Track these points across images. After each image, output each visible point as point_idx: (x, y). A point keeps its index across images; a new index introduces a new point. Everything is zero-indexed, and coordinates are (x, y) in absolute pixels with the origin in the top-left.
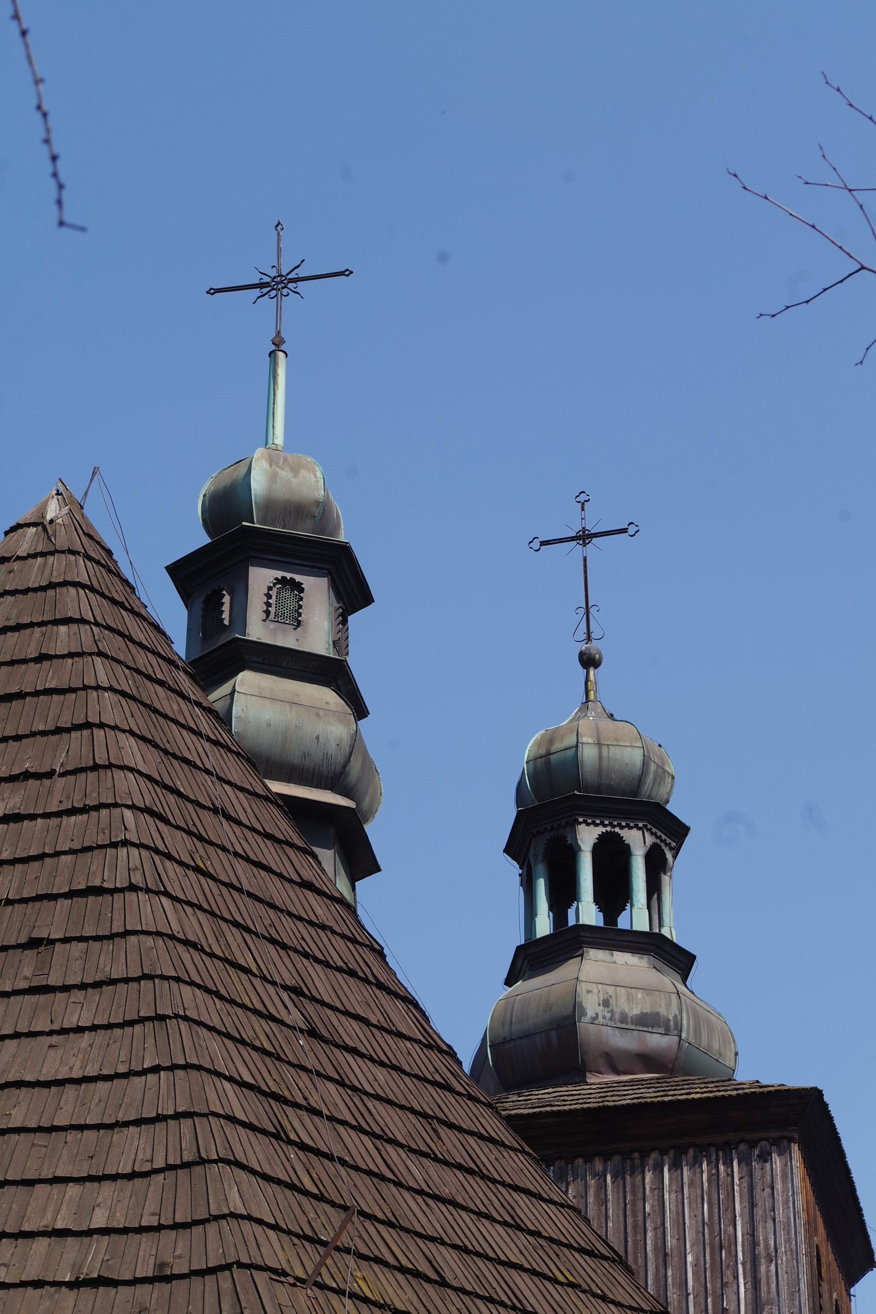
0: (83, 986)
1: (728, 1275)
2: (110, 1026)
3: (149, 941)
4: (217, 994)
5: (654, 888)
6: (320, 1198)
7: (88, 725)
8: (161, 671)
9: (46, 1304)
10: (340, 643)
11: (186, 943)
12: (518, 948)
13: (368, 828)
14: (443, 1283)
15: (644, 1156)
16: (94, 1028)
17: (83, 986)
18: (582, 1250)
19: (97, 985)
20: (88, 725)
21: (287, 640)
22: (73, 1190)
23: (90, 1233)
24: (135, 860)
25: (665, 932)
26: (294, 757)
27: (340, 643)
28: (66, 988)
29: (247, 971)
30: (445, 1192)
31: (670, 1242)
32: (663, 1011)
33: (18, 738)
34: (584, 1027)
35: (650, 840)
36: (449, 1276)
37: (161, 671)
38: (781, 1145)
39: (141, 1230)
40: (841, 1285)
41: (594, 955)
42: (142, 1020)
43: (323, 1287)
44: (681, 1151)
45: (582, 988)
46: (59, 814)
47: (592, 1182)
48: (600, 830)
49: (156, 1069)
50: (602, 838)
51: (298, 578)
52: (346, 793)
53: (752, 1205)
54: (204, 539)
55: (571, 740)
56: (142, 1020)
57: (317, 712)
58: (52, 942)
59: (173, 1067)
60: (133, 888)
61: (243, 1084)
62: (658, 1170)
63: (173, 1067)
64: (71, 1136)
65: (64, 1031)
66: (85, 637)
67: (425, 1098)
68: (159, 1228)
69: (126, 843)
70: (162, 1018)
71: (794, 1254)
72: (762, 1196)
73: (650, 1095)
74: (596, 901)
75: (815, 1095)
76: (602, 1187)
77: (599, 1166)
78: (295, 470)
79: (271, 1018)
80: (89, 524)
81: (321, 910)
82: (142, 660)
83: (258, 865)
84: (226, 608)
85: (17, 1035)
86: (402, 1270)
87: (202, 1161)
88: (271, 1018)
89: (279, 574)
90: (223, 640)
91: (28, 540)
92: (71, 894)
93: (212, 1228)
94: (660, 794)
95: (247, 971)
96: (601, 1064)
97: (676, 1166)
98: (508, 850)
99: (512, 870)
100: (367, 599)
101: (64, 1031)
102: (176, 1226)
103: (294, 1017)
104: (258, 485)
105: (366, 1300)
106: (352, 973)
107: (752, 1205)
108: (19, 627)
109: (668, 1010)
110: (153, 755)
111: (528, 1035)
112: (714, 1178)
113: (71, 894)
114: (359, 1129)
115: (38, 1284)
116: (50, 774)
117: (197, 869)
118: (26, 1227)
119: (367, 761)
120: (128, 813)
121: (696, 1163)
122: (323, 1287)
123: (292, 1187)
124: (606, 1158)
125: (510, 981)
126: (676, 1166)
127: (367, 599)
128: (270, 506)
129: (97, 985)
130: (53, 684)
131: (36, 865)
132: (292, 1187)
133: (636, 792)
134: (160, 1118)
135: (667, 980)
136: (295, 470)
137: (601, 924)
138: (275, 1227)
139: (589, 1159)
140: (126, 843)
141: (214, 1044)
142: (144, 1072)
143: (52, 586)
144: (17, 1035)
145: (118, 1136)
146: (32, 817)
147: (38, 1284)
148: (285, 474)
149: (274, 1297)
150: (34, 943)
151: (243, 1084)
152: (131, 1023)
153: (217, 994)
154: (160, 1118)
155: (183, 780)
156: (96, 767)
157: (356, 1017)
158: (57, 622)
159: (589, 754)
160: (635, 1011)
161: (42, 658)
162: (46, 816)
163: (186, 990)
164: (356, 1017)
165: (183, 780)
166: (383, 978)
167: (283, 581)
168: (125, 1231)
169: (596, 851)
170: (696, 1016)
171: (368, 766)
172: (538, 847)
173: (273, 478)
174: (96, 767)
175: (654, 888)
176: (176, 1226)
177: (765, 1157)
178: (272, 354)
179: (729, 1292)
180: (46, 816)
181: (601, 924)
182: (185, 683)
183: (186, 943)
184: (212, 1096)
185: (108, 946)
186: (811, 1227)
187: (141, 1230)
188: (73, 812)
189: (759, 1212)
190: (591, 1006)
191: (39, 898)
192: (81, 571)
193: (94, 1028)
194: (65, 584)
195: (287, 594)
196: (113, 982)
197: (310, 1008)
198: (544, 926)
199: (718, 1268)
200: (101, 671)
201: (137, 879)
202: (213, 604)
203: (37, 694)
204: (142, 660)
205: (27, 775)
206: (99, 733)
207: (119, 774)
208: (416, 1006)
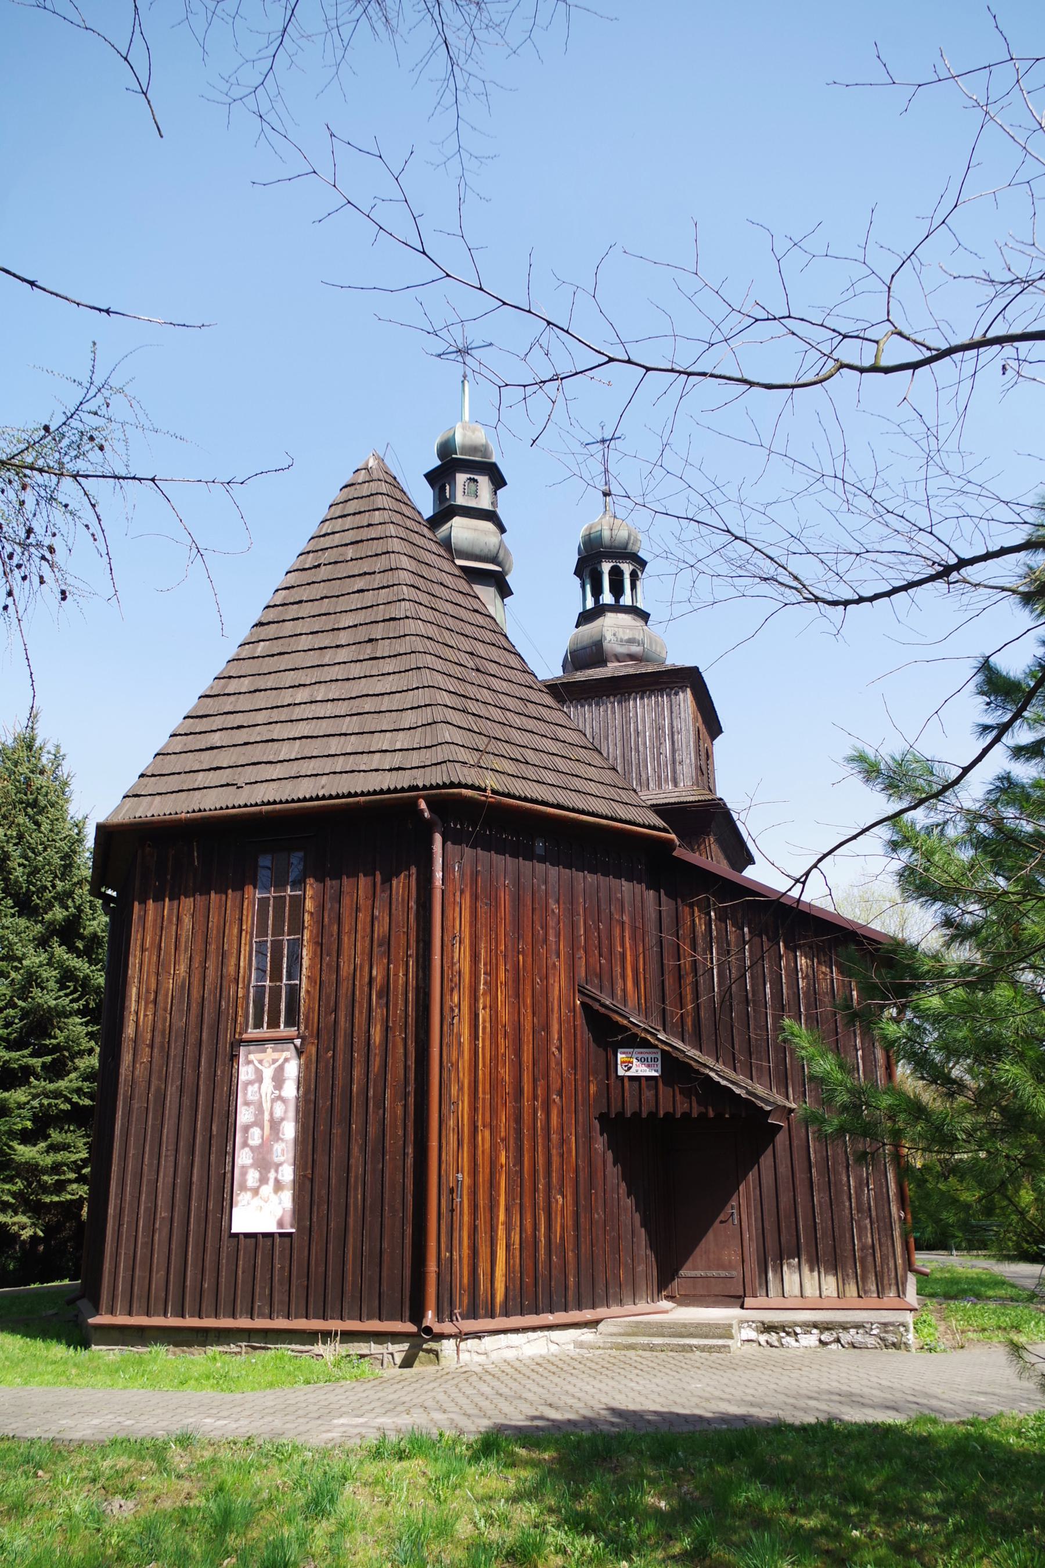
0: (390, 657)
1: (662, 740)
2: (400, 672)
3: (414, 638)
4: (440, 657)
5: (633, 587)
6: (480, 734)
7: (388, 552)
8: (416, 527)
9: (380, 777)
10: (494, 504)
11: (428, 638)
12: (580, 614)
13: (507, 578)
14: (527, 763)
15: (630, 695)
16: (394, 673)
17: (390, 657)
18: (582, 747)
19: (395, 656)
20: (388, 552)
21: (472, 503)
22: (388, 734)
23: (395, 751)
24: (408, 607)
25: (638, 605)
26: (477, 551)
27: (494, 504)
28: (383, 658)
29: (452, 647)
30: (529, 728)
31: (640, 728)
32: (637, 637)
33: (361, 558)
34: (606, 644)
35: (632, 567)
36: (529, 760)
37: (416, 527)
38: (683, 688)
39: (413, 749)
40: (708, 740)
41: (609, 615)
42: (412, 669)
43: (481, 767)
44: (644, 692)
45: (605, 629)
46: (378, 589)
47: (609, 706)
48: (612, 564)
49: (417, 688)
50: (613, 568)
51: (476, 477)
52: (499, 564)
53: (672, 712)
54: (439, 463)
55: (599, 528)
56: (412, 669)
57: (486, 532)
58: (377, 640)
59: (424, 687)
60: (407, 617)
61: (450, 692)
62: (635, 699)
63: (424, 687)
64: (387, 714)
65: (383, 675)
66: (385, 516)
67: (153, 986)
68: (420, 748)
69: (404, 600)
70: (419, 668)
71: (688, 730)
72: (675, 709)
73: (631, 671)
74: (611, 591)
75: (695, 670)
76: (613, 707)
77: (612, 699)
78: (473, 432)
79: (462, 665)
80: (386, 467)
81: (480, 620)
82: (409, 523)
83: (456, 604)
84: (448, 491)
85: (365, 677)
86: (511, 759)
87: (435, 723)
88: (462, 665)
89: (469, 476)
90: (447, 504)
91: (362, 476)
92: (384, 621)
93: (439, 747)
94: (635, 549)
95: (452, 647)
96: (613, 659)
97: (642, 698)
98: (575, 573)
99: (577, 581)
100: (505, 484)
101: (383, 675)
102: (426, 747)
103: (471, 664)
104: (459, 440)
105: (497, 771)
106: (494, 645)
107: (672, 712)
108: (360, 513)
109: (639, 636)
110: (414, 563)
111: (584, 648)
112: (657, 702)
113: (384, 621)
114: (496, 706)
115: (377, 770)
116: (374, 573)
117: (432, 608)
118: (372, 750)
119: (506, 550)
120: (404, 587)
121: (650, 697)
122: (481, 767)
123: (469, 730)
124: (615, 696)
125: (577, 627)
126: (642, 698)
127: (505, 484)
128: (465, 449)
129: (395, 656)
130: (373, 536)
131: (370, 609)
132: (469, 730)
133: (626, 548)
134: (419, 707)
135: (640, 623)
136: (473, 432)
137: (613, 602)
138: (463, 746)
139: (608, 697)
140: (404, 600)
141: (439, 677)
142: (413, 689)
143: (372, 495)
144: (365, 677)
145: (404, 714)
146: (368, 590)
147: (377, 770)
148: (469, 433)
149: (462, 772)
150: (370, 640)
151: (450, 692)
152: (408, 671)
153: (440, 657)
154: (419, 707)
155: (425, 571)
156: (391, 569)
157: (495, 662)
158: (374, 510)
159: (606, 534)
160: (626, 637)
161: (369, 525)
162: (373, 589)
163: (428, 656)
164: (495, 662)
165: (425, 571)
166: (506, 645)
167: (470, 479)
168: (408, 750)
169: (611, 573)
170: (650, 638)
171: (507, 553)
172: (587, 572)
173: (464, 435)
174: (391, 569)
175: (633, 587)
176: (426, 747)
177: (676, 694)
178: (463, 382)
179: (663, 746)
180: (373, 589)
181: (613, 602)
182: (426, 531)
183: (428, 638)
184: (438, 697)
185: (399, 640)
186: (695, 719)
187: (413, 749)
188: (383, 587)
189: (674, 715)
190: (609, 636)
191: (372, 623)
192: (384, 488)
193: (394, 673)
194: (377, 494)
195: (472, 484)
196: (401, 655)
197: (477, 660)
198: (590, 604)
199: (658, 737)
200: (392, 530)
201: (409, 614)
202: (442, 489)
203: (368, 540)
204: (409, 523)
205: (365, 574)
206: (392, 555)
207: (401, 572)
208: (519, 655)
